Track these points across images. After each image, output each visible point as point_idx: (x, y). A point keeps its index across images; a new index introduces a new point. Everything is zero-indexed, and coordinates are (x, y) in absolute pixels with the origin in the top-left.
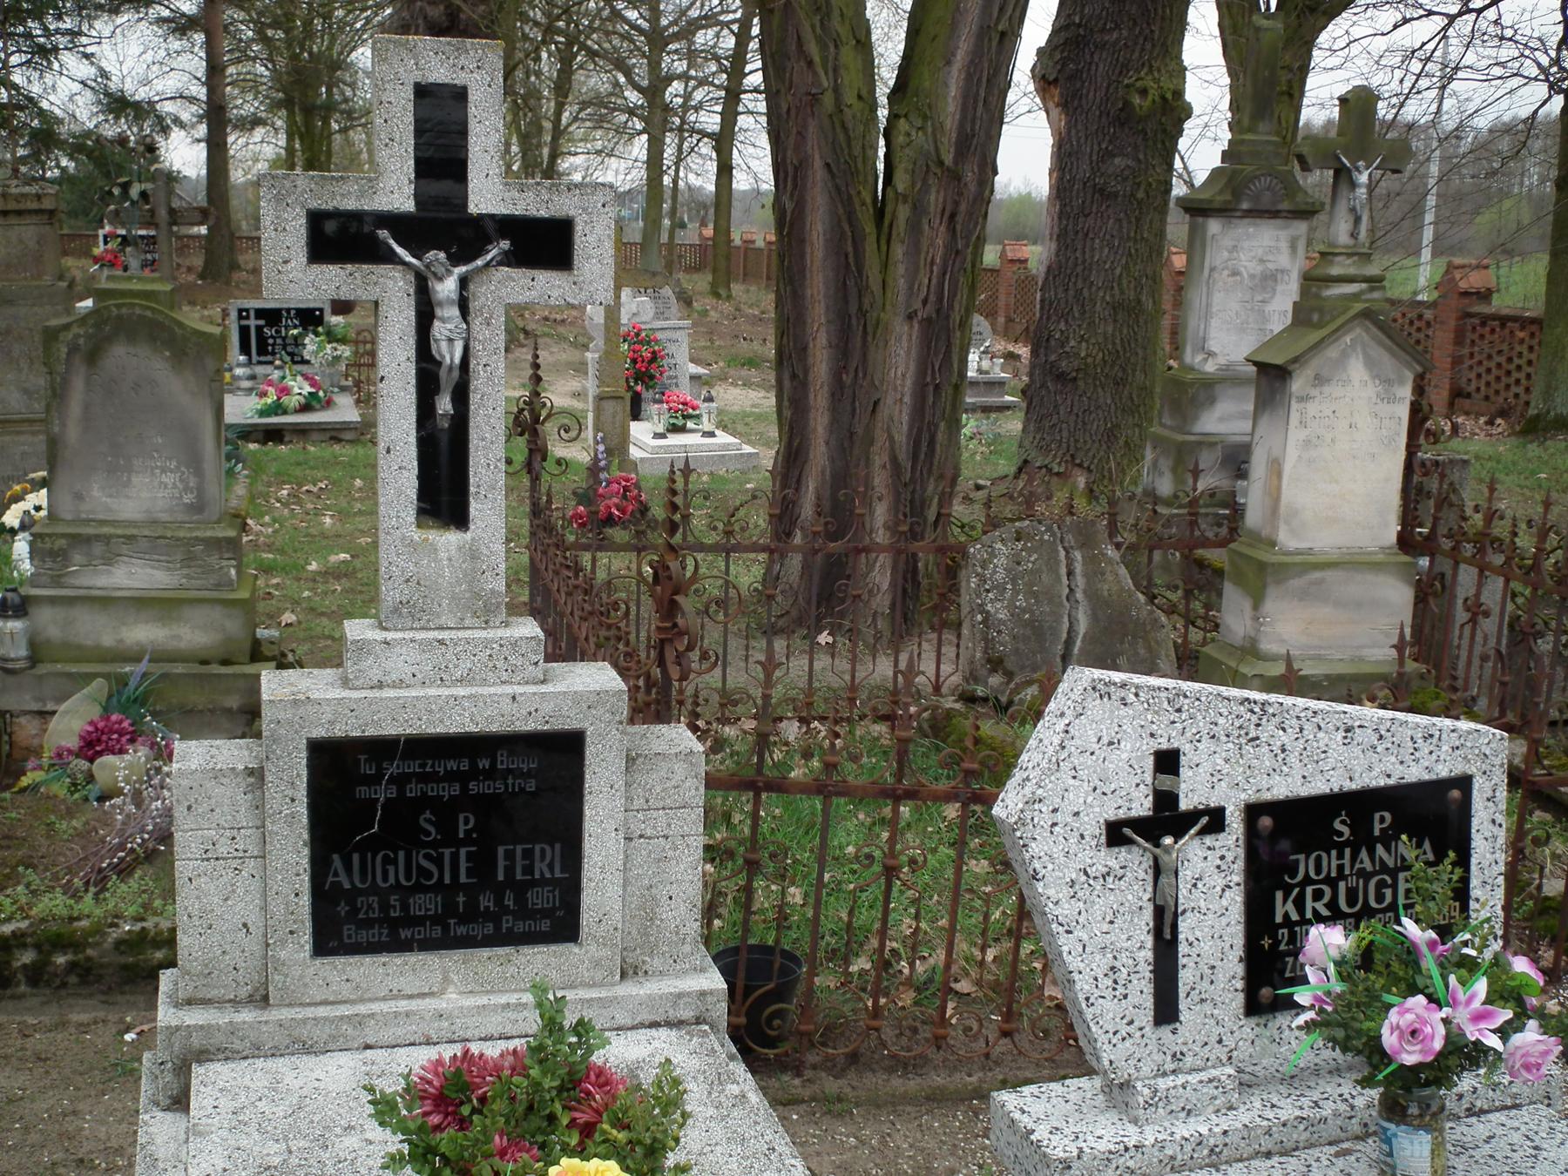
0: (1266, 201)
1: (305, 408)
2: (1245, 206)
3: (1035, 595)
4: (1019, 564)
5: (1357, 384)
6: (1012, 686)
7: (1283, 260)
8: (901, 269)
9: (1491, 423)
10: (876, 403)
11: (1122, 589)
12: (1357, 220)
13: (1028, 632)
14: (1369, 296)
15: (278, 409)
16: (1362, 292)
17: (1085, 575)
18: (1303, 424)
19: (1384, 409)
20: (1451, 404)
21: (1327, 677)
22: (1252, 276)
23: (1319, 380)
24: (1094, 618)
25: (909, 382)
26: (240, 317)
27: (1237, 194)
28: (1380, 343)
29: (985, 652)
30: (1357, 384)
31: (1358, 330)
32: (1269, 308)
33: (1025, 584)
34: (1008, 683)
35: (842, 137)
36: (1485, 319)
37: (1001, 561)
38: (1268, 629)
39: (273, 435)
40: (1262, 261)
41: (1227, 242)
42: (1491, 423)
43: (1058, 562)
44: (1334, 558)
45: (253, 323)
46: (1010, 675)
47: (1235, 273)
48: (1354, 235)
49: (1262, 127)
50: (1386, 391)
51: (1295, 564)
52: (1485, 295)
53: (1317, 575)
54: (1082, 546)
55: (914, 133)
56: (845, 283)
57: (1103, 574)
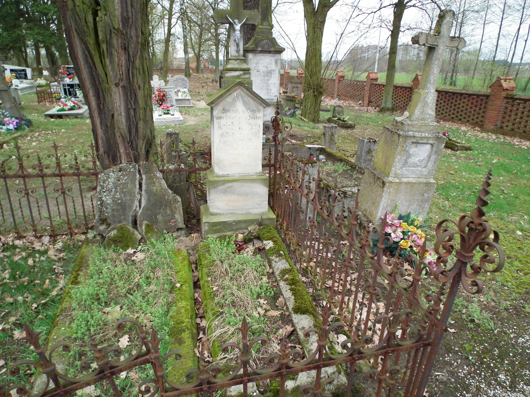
0: (266, 48)
1: (71, 109)
2: (259, 49)
3: (124, 193)
4: (119, 181)
5: (240, 112)
6: (109, 229)
7: (273, 67)
8: (110, 68)
9: (375, 108)
10: (113, 115)
11: (162, 189)
12: (238, 45)
13: (119, 207)
14: (244, 77)
15: (63, 110)
16: (241, 75)
17: (146, 184)
18: (220, 128)
19: (253, 121)
20: (368, 104)
21: (234, 221)
22: (264, 72)
23: (225, 110)
24: (149, 200)
25: (122, 108)
26: (63, 86)
27: (257, 46)
28: (248, 96)
29: (100, 216)
30: (240, 112)
31: (239, 91)
32: (269, 82)
33: (120, 189)
34: (107, 228)
35: (77, 18)
36: (376, 85)
37: (111, 180)
38: (212, 204)
39: (60, 117)
40: (266, 67)
41: (255, 61)
42: (375, 108)
43: (135, 180)
44: (236, 178)
45: (67, 87)
46: (109, 225)
47: (258, 71)
48: (238, 51)
49: (265, 23)
50: (253, 115)
51: (220, 181)
52: (376, 79)
53: (230, 184)
54: (146, 173)
55: (103, 16)
56: (92, 73)
57: (154, 183)
